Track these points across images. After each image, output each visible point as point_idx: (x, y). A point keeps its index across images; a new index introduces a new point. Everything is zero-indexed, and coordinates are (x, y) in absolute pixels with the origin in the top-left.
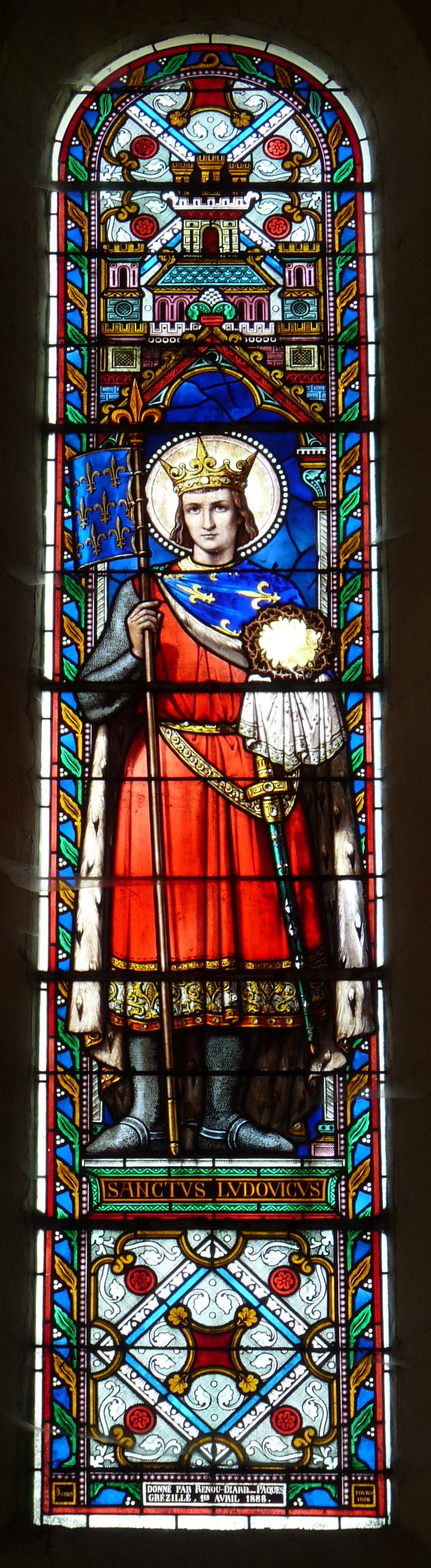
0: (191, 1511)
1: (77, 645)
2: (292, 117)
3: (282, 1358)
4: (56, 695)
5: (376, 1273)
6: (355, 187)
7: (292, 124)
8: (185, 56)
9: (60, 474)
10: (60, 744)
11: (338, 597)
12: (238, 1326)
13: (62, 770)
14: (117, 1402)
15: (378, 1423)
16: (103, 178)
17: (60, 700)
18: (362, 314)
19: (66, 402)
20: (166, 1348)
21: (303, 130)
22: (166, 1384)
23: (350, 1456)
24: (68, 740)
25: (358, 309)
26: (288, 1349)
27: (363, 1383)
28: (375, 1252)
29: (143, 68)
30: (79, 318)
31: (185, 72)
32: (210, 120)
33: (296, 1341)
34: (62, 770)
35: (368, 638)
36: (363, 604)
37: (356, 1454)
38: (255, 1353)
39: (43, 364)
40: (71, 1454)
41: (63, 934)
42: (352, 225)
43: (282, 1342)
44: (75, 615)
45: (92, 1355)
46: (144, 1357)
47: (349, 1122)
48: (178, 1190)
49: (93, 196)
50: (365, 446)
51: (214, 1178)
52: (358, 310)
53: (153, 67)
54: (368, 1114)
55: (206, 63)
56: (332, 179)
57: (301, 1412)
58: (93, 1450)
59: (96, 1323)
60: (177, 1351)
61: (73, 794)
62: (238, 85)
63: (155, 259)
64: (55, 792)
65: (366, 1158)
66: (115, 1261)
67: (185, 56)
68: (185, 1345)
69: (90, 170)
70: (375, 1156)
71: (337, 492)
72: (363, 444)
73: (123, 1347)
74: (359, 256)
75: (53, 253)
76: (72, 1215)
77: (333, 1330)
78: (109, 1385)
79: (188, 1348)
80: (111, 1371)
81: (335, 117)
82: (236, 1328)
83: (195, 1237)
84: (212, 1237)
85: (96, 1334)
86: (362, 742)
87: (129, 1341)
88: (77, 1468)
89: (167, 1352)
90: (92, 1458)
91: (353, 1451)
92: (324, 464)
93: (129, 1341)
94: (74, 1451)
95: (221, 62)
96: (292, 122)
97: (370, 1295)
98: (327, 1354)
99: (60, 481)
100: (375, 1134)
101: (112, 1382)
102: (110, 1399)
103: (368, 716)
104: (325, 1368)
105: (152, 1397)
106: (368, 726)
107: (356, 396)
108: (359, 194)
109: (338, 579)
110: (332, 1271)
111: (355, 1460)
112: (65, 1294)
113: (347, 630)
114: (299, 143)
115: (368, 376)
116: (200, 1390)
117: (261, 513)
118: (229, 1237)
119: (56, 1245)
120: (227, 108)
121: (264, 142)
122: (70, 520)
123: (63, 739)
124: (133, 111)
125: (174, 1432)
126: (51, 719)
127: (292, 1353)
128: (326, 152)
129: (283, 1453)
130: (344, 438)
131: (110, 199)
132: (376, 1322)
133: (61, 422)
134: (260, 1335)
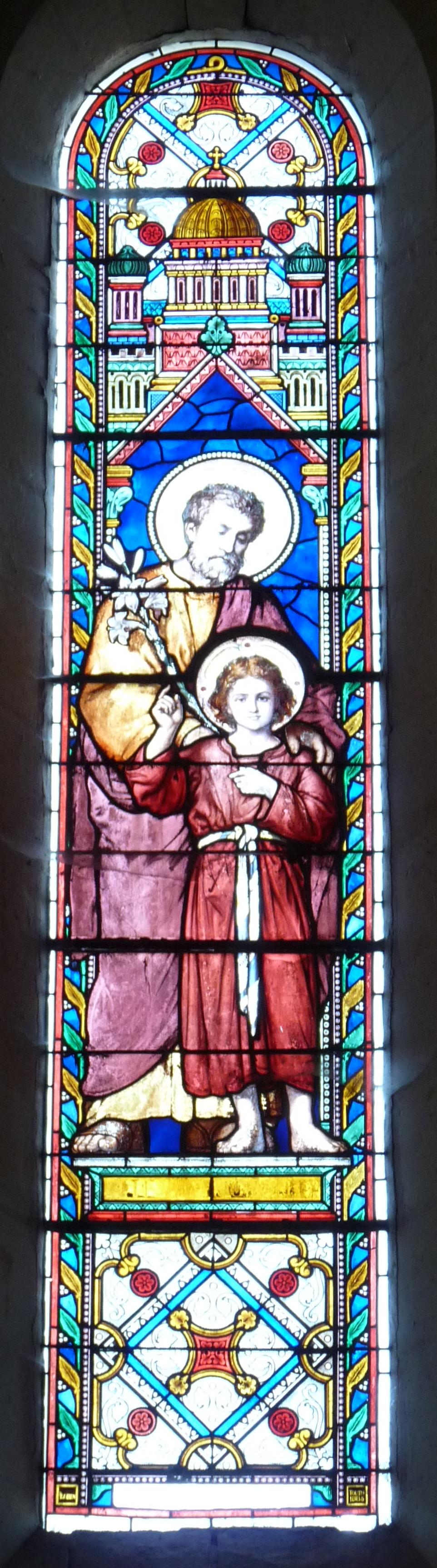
1: (72, 1389)
2: (298, 119)
8: (191, 59)
9: (67, 611)
10: (74, 409)
13: (61, 1335)
16: (113, 187)
17: (74, 452)
18: (368, 701)
19: (73, 493)
23: (345, 1457)
24: (80, 532)
26: (285, 1350)
27: (355, 777)
29: (150, 71)
30: (87, 327)
31: (189, 77)
33: (294, 1343)
34: (61, 1335)
36: (359, 315)
37: (351, 1457)
39: (43, 1068)
40: (74, 1456)
44: (73, 1263)
45: (95, 1356)
47: (348, 1272)
49: (99, 445)
52: (364, 740)
53: (159, 71)
56: (335, 182)
62: (246, 88)
64: (70, 411)
65: (359, 661)
67: (191, 59)
69: (98, 181)
71: (344, 1267)
73: (126, 1350)
74: (361, 258)
76: (75, 1219)
77: (331, 1333)
81: (340, 121)
83: (199, 1239)
86: (354, 158)
91: (348, 1453)
92: (323, 275)
94: (77, 1452)
95: (226, 65)
97: (362, 1016)
98: (324, 1355)
103: (364, 380)
105: (164, 136)
106: (364, 387)
108: (360, 197)
109: (344, 1360)
110: (331, 1275)
111: (349, 1461)
117: (263, 205)
118: (230, 1241)
120: (234, 111)
121: (268, 146)
123: (77, 404)
124: (142, 116)
128: (338, 1103)
130: (342, 201)
131: (117, 206)
133: (71, 430)
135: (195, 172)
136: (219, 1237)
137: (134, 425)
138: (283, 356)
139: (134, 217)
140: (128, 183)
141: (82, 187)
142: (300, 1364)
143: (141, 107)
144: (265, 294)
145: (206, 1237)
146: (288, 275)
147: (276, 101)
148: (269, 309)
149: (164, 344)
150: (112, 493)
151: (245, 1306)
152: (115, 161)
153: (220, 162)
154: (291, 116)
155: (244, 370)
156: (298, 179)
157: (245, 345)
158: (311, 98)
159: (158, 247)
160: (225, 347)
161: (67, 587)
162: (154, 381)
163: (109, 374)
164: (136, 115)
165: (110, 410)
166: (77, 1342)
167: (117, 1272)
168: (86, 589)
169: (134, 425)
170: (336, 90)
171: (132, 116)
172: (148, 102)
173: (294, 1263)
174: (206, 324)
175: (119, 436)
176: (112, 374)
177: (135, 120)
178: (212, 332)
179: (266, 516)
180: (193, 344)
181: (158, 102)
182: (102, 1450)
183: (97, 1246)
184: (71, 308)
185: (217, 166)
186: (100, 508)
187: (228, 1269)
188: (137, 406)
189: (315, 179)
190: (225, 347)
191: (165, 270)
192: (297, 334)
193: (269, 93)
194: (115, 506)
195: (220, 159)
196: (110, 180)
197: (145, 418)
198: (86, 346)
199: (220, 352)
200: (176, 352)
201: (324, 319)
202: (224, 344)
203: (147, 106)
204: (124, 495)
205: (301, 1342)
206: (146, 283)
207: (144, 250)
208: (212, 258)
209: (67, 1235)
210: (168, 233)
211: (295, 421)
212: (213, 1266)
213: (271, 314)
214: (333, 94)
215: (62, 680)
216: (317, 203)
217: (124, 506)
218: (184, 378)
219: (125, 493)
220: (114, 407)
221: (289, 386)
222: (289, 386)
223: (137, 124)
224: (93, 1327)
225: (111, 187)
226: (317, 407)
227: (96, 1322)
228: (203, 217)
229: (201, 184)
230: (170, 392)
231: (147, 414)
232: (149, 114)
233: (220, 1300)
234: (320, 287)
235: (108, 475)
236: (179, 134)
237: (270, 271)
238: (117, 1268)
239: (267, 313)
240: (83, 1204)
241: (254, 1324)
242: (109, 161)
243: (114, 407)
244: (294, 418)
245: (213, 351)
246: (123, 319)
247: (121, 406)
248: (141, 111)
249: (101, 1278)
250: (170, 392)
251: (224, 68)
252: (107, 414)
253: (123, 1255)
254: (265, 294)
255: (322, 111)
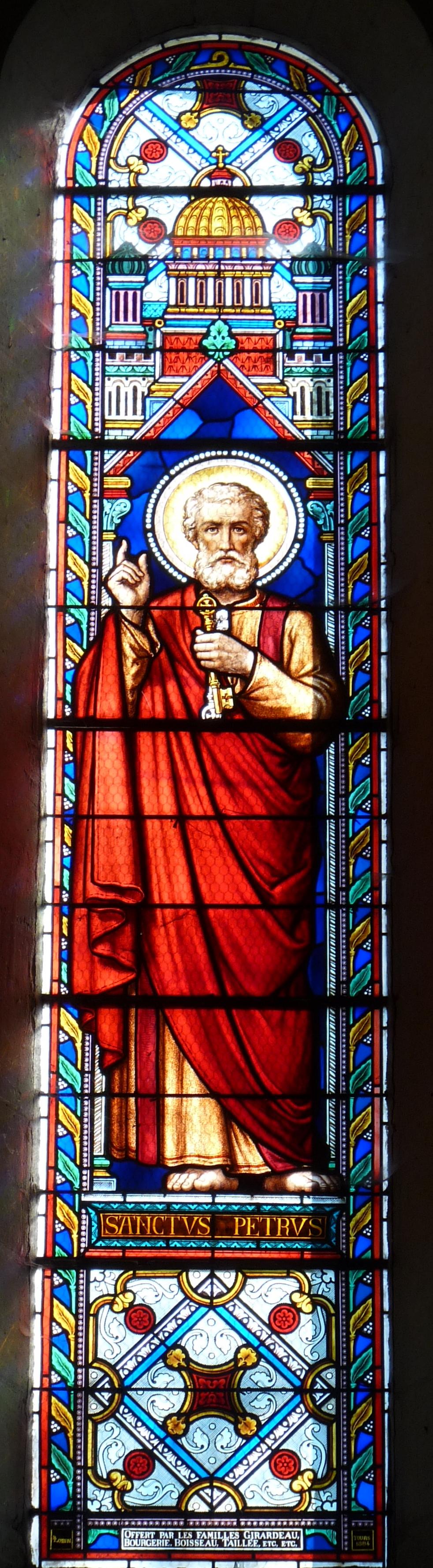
0: (190, 1555)
3: (282, 1399)
4: (64, 454)
5: (375, 751)
6: (368, 190)
7: (304, 127)
11: (346, 531)
12: (235, 1367)
14: (117, 1445)
15: (374, 524)
17: (68, 458)
19: (71, 371)
20: (166, 1389)
21: (317, 136)
22: (178, 120)
23: (350, 1499)
25: (368, 319)
28: (375, 1293)
32: (221, 121)
33: (297, 1383)
35: (375, 756)
37: (356, 1499)
38: (254, 1394)
40: (68, 1499)
41: (71, 647)
42: (364, 272)
43: (281, 1383)
45: (91, 1399)
46: (143, 1399)
48: (180, 1228)
50: (375, 688)
51: (213, 1239)
54: (372, 1448)
55: (215, 62)
57: (299, 1454)
58: (90, 1495)
59: (95, 1365)
60: (175, 1392)
61: (82, 510)
62: (250, 86)
63: (162, 266)
66: (114, 1300)
68: (182, 1386)
69: (97, 181)
70: (375, 683)
72: (372, 463)
73: (121, 1390)
75: (52, 607)
78: (108, 1427)
79: (185, 1389)
80: (110, 1413)
82: (236, 1369)
83: (196, 1277)
84: (212, 1276)
85: (95, 1375)
86: (369, 772)
87: (127, 1382)
88: (73, 1514)
89: (165, 1393)
90: (89, 1503)
91: (353, 1495)
93: (127, 1382)
96: (304, 123)
99: (56, 956)
100: (378, 1371)
101: (111, 1423)
102: (109, 1442)
103: (377, 1120)
104: (324, 1409)
107: (366, 499)
108: (374, 453)
111: (353, 1504)
112: (62, 1436)
113: (356, 698)
114: (310, 143)
115: (377, 303)
116: (199, 1432)
118: (228, 1277)
119: (59, 1140)
122: (72, 765)
125: (170, 1476)
126: (62, 389)
127: (292, 1394)
129: (281, 1498)
132: (378, 1366)
134: (260, 1376)
135: (198, 172)
136: (219, 1274)
137: (131, 433)
138: (289, 363)
139: (132, 214)
140: (129, 182)
141: (81, 185)
142: (302, 1402)
143: (143, 104)
144: (270, 298)
145: (205, 1274)
146: (295, 278)
147: (282, 100)
148: (274, 314)
149: (162, 350)
150: (110, 505)
151: (244, 1342)
152: (115, 159)
153: (223, 162)
154: (297, 115)
155: (247, 376)
156: (307, 178)
157: (249, 351)
158: (319, 97)
159: (158, 243)
160: (227, 353)
161: (67, 258)
162: (153, 388)
163: (106, 378)
164: (136, 113)
165: (107, 417)
166: (71, 1383)
167: (111, 1309)
168: (75, 1094)
169: (131, 433)
170: (344, 88)
171: (132, 114)
172: (150, 98)
173: (296, 1297)
174: (208, 327)
175: (117, 445)
176: (109, 379)
177: (137, 119)
178: (215, 338)
179: (269, 530)
180: (195, 350)
181: (159, 99)
182: (97, 1493)
183: (92, 1279)
184: (66, 392)
185: (221, 165)
186: (96, 518)
187: (227, 1306)
188: (135, 413)
189: (324, 178)
190: (227, 353)
191: (167, 269)
192: (303, 340)
193: (274, 91)
194: (113, 517)
195: (224, 158)
196: (110, 178)
197: (143, 425)
198: (84, 350)
199: (222, 357)
200: (178, 358)
201: (331, 325)
202: (227, 350)
203: (148, 104)
204: (121, 508)
205: (303, 1381)
206: (147, 282)
207: (143, 248)
208: (214, 259)
209: (60, 1271)
210: (169, 231)
211: (300, 430)
212: (212, 1302)
213: (276, 320)
214: (342, 93)
215: (59, 724)
216: (324, 202)
217: (123, 518)
218: (184, 384)
219: (123, 506)
220: (110, 414)
221: (295, 393)
222: (295, 393)
223: (138, 122)
224: (88, 1366)
225: (110, 185)
226: (324, 416)
227: (90, 1360)
228: (207, 212)
229: (206, 183)
230: (169, 398)
231: (145, 421)
232: (150, 111)
233: (218, 1337)
234: (327, 291)
235: (105, 486)
236: (182, 133)
237: (275, 274)
238: (112, 1304)
239: (272, 318)
240: (79, 1242)
241: (243, 1433)
242: (109, 158)
243: (110, 414)
244: (299, 427)
245: (216, 357)
246: (122, 320)
247: (118, 413)
248: (142, 108)
249: (96, 1315)
250: (169, 398)
251: (229, 63)
252: (104, 421)
253: (119, 1291)
254: (270, 298)
255: (328, 106)
